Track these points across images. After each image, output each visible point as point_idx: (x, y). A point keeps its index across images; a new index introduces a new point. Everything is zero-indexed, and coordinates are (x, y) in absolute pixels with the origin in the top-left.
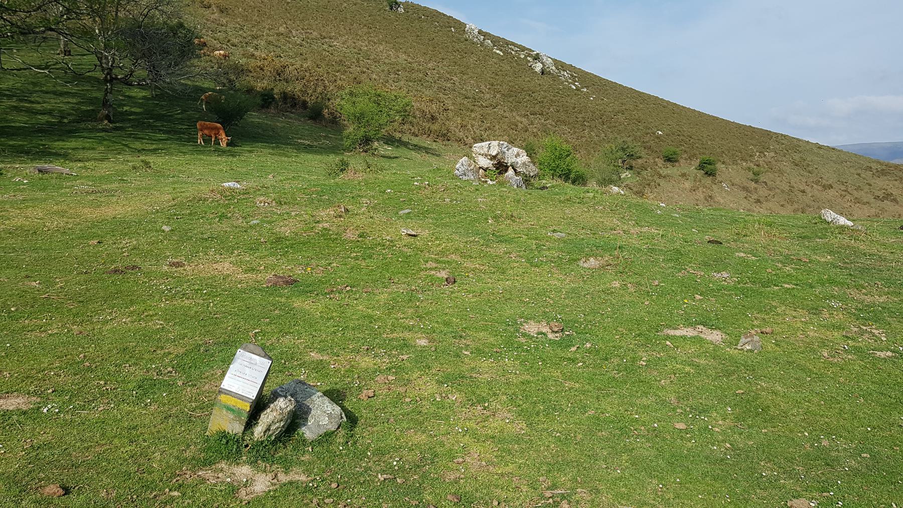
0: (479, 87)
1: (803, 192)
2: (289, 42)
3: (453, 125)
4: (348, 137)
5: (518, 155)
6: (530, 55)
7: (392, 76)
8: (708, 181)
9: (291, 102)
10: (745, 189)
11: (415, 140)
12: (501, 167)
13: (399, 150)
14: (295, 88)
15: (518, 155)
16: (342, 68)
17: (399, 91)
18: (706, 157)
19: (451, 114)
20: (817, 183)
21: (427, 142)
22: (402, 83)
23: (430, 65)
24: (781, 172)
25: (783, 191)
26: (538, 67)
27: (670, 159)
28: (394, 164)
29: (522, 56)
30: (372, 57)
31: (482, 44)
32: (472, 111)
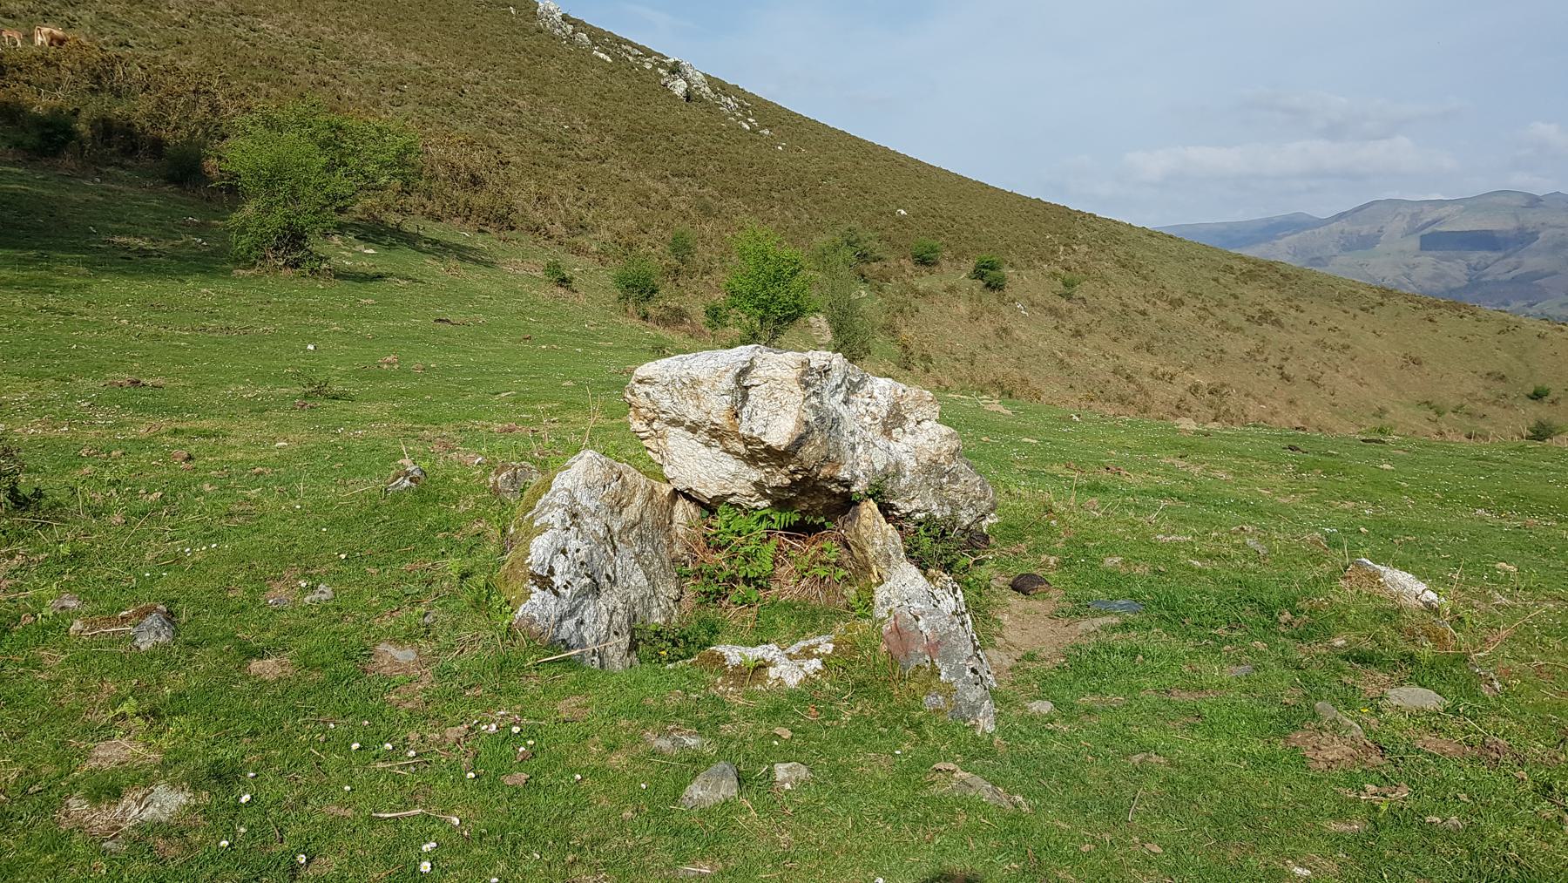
0: (569, 120)
1: (1144, 313)
2: (155, 17)
3: (521, 197)
4: (243, 230)
5: (894, 419)
6: (662, 65)
7: (389, 93)
8: (991, 298)
9: (120, 142)
10: (1052, 311)
11: (434, 230)
12: (812, 500)
13: (394, 253)
14: (138, 110)
15: (894, 419)
16: (274, 75)
17: (394, 124)
18: (986, 256)
19: (514, 173)
20: (1160, 296)
21: (463, 234)
22: (410, 107)
23: (468, 76)
24: (1105, 281)
25: (1112, 314)
26: (679, 87)
27: (925, 261)
28: (368, 298)
29: (649, 67)
30: (345, 55)
31: (571, 40)
32: (558, 167)
